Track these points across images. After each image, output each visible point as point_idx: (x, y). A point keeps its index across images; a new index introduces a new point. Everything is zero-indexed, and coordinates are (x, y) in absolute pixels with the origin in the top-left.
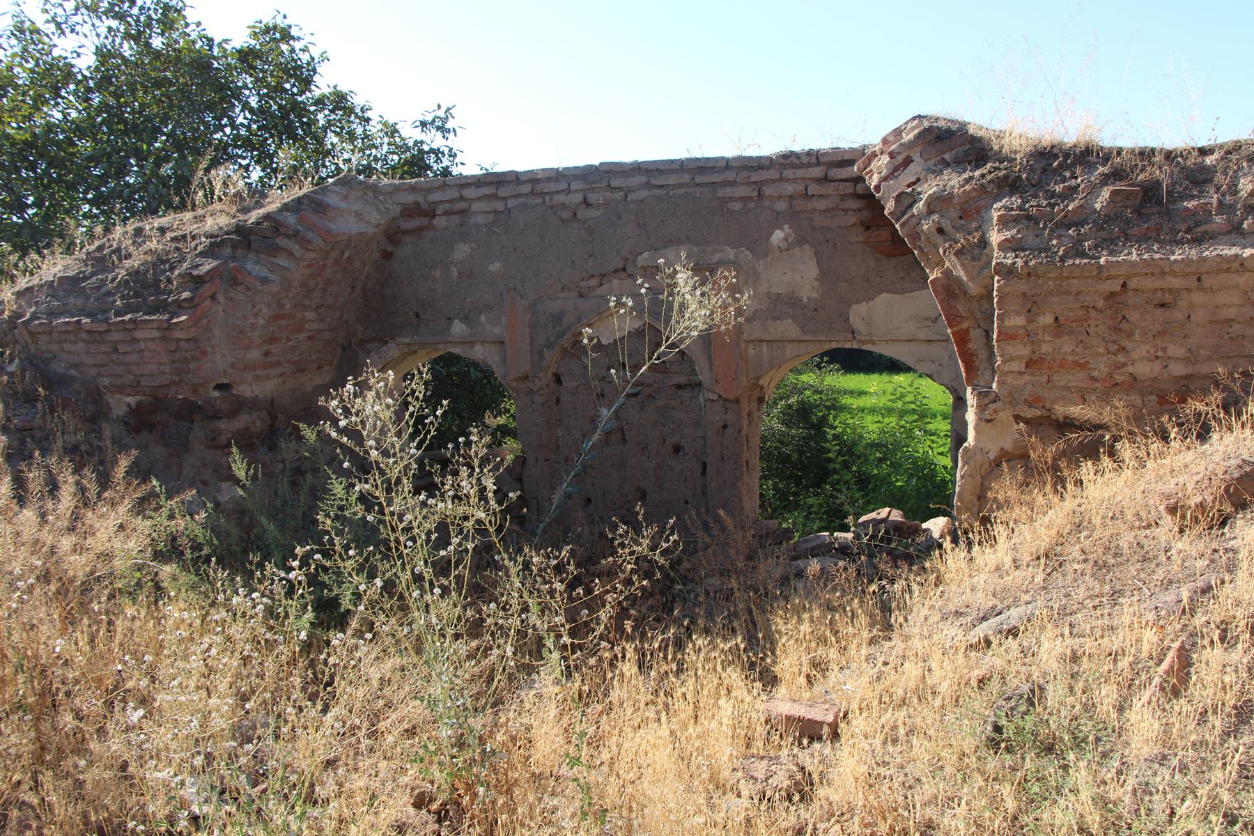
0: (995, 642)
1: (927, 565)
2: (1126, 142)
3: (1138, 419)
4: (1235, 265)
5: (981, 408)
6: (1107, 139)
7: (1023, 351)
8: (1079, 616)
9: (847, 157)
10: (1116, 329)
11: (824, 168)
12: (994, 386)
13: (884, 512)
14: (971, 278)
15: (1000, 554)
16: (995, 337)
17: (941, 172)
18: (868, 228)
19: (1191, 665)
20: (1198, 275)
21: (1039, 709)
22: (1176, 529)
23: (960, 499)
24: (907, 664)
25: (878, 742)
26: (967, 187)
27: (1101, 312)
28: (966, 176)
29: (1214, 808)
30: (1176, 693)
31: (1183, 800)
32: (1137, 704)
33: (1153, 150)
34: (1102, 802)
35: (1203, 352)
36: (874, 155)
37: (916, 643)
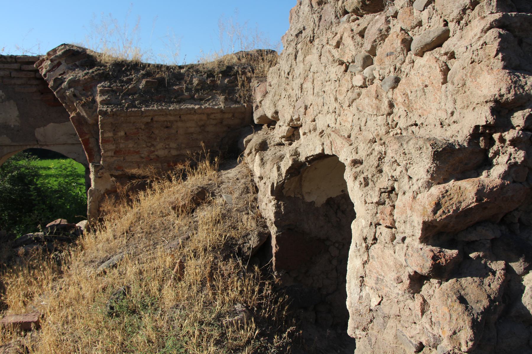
0: (108, 271)
1: (77, 242)
2: (152, 62)
3: (159, 174)
4: (193, 112)
5: (96, 172)
6: (144, 60)
7: (113, 147)
8: (141, 255)
9: (30, 60)
10: (150, 137)
11: (19, 65)
12: (101, 162)
13: (58, 221)
14: (89, 116)
15: (108, 234)
16: (100, 141)
17: (74, 70)
18: (42, 94)
19: (184, 268)
20: (179, 114)
21: (128, 296)
22: (176, 215)
23: (90, 212)
24: (70, 288)
25: (60, 325)
26: (86, 77)
27: (143, 130)
28: (85, 72)
29: (196, 320)
30: (180, 280)
31: (185, 320)
32: (166, 287)
33: (162, 65)
34: (156, 328)
35: (183, 145)
36: (43, 60)
37: (74, 278)
